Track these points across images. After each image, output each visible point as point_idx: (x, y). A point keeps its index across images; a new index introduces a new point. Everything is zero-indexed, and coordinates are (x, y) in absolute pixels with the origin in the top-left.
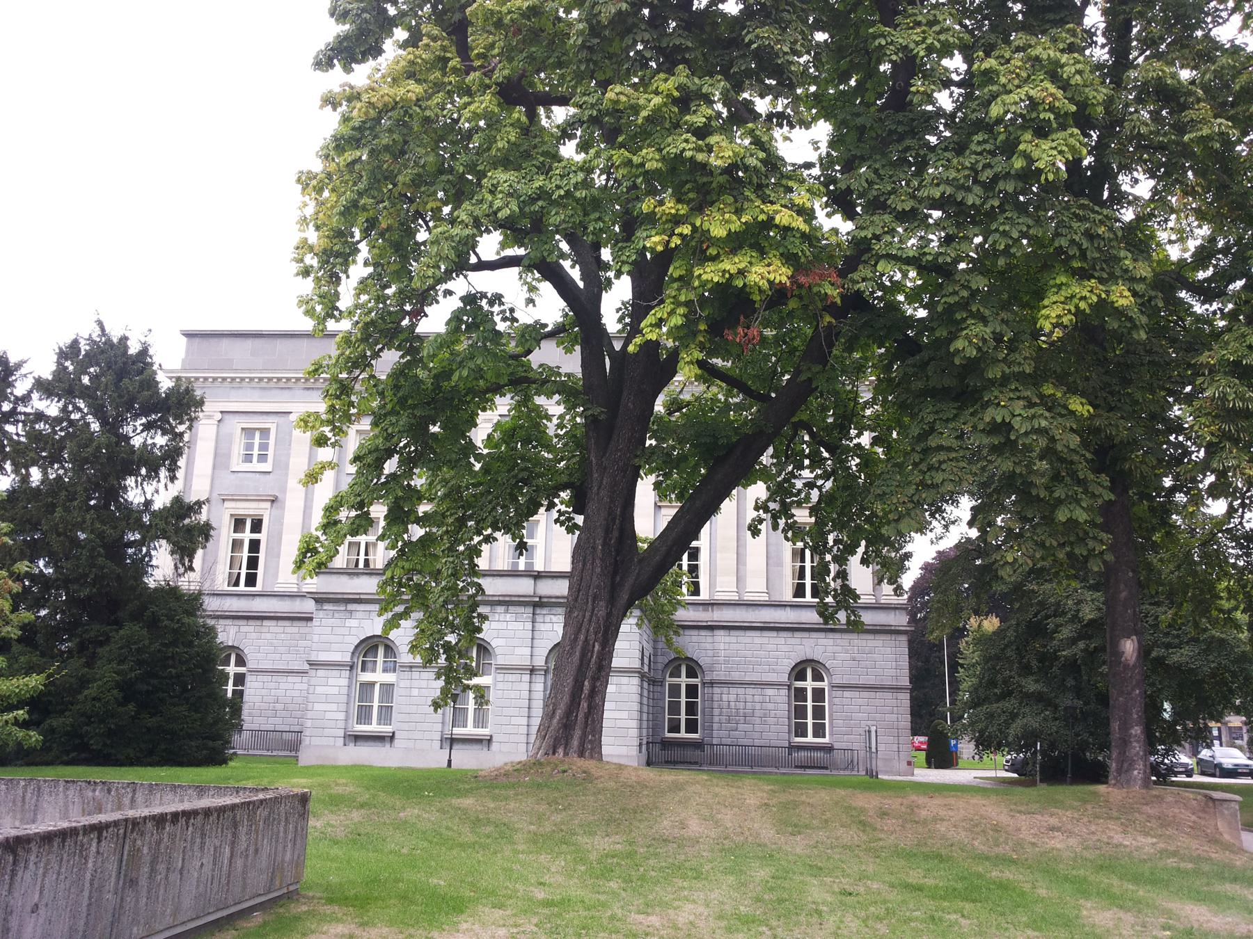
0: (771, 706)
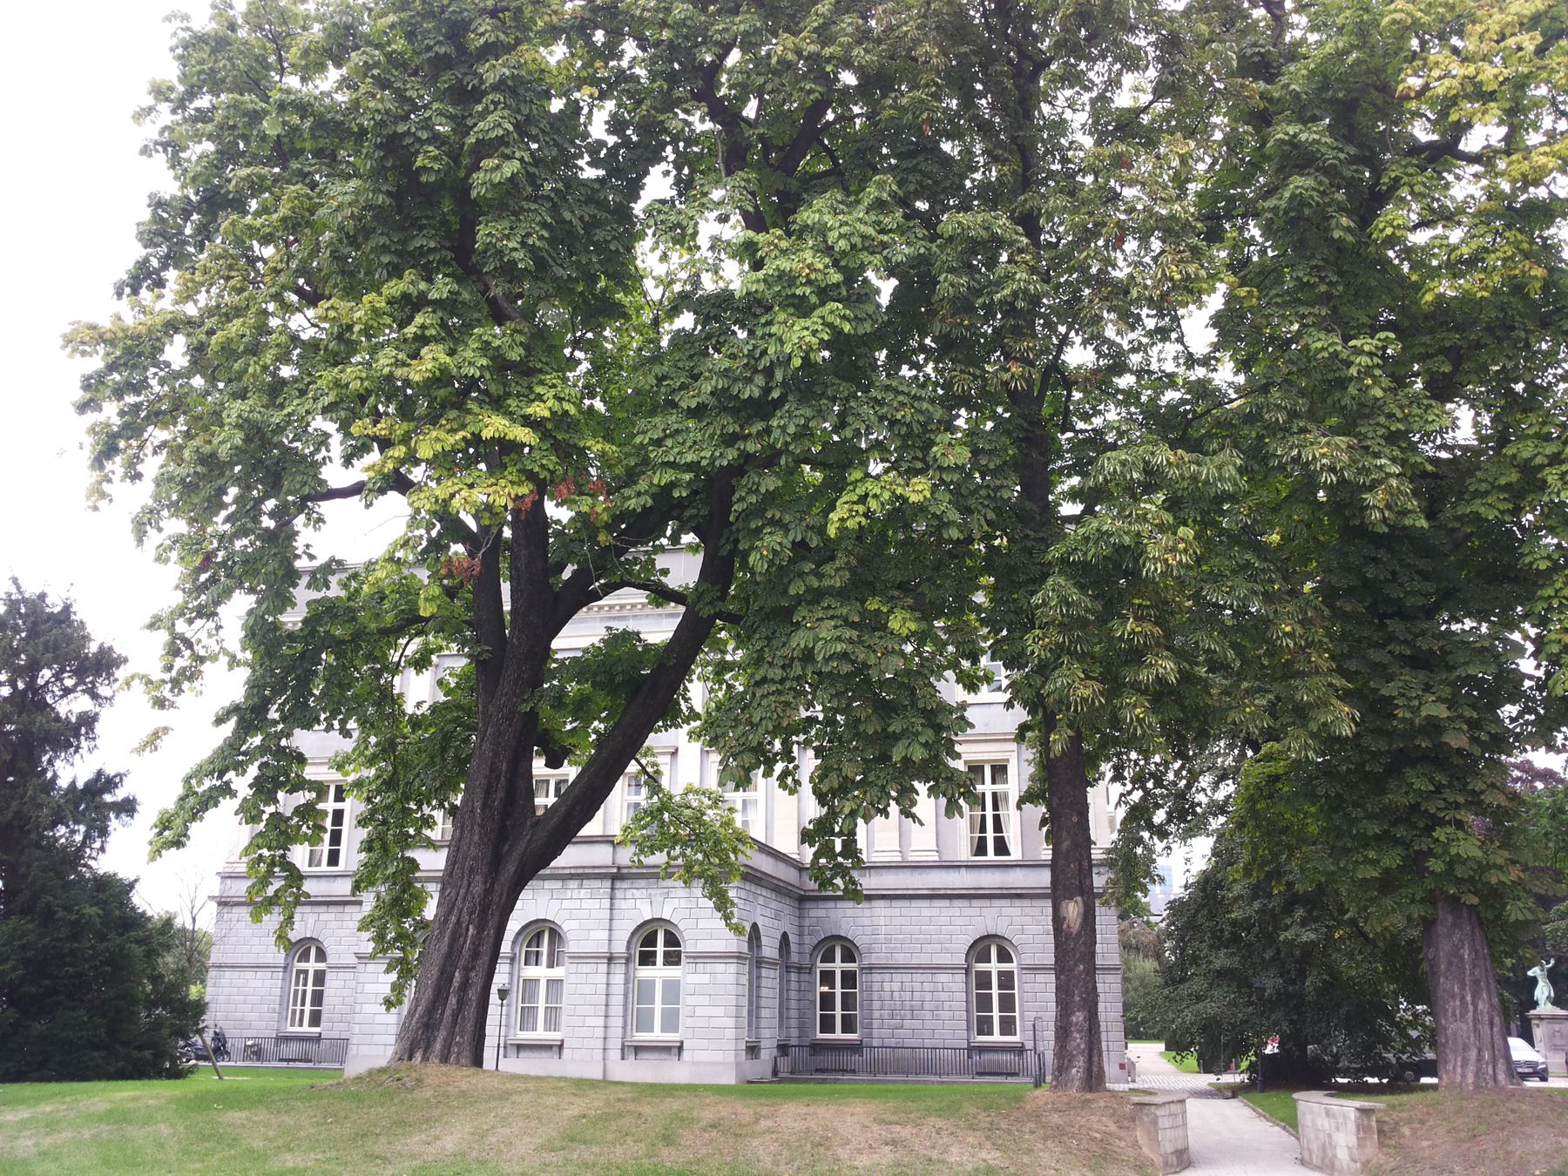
0: (944, 996)
